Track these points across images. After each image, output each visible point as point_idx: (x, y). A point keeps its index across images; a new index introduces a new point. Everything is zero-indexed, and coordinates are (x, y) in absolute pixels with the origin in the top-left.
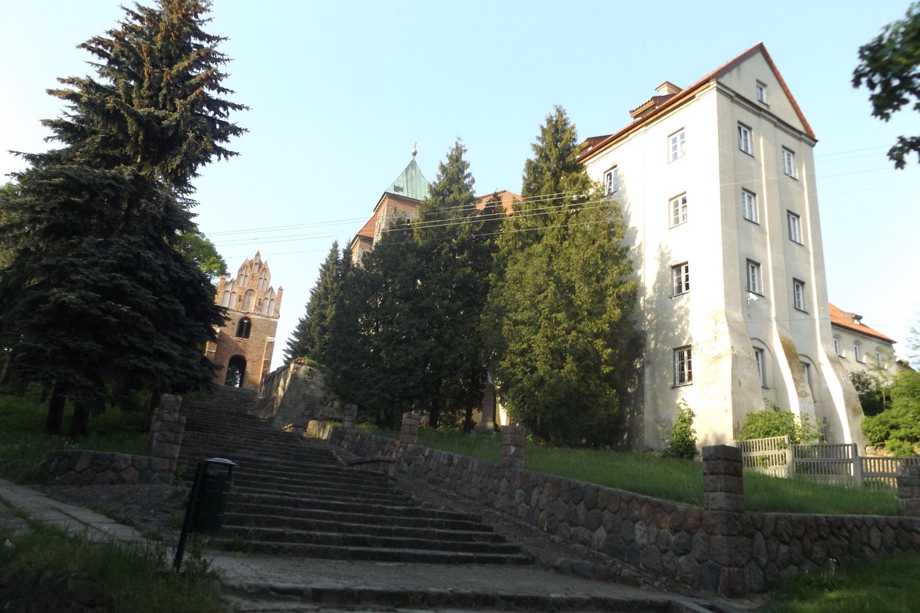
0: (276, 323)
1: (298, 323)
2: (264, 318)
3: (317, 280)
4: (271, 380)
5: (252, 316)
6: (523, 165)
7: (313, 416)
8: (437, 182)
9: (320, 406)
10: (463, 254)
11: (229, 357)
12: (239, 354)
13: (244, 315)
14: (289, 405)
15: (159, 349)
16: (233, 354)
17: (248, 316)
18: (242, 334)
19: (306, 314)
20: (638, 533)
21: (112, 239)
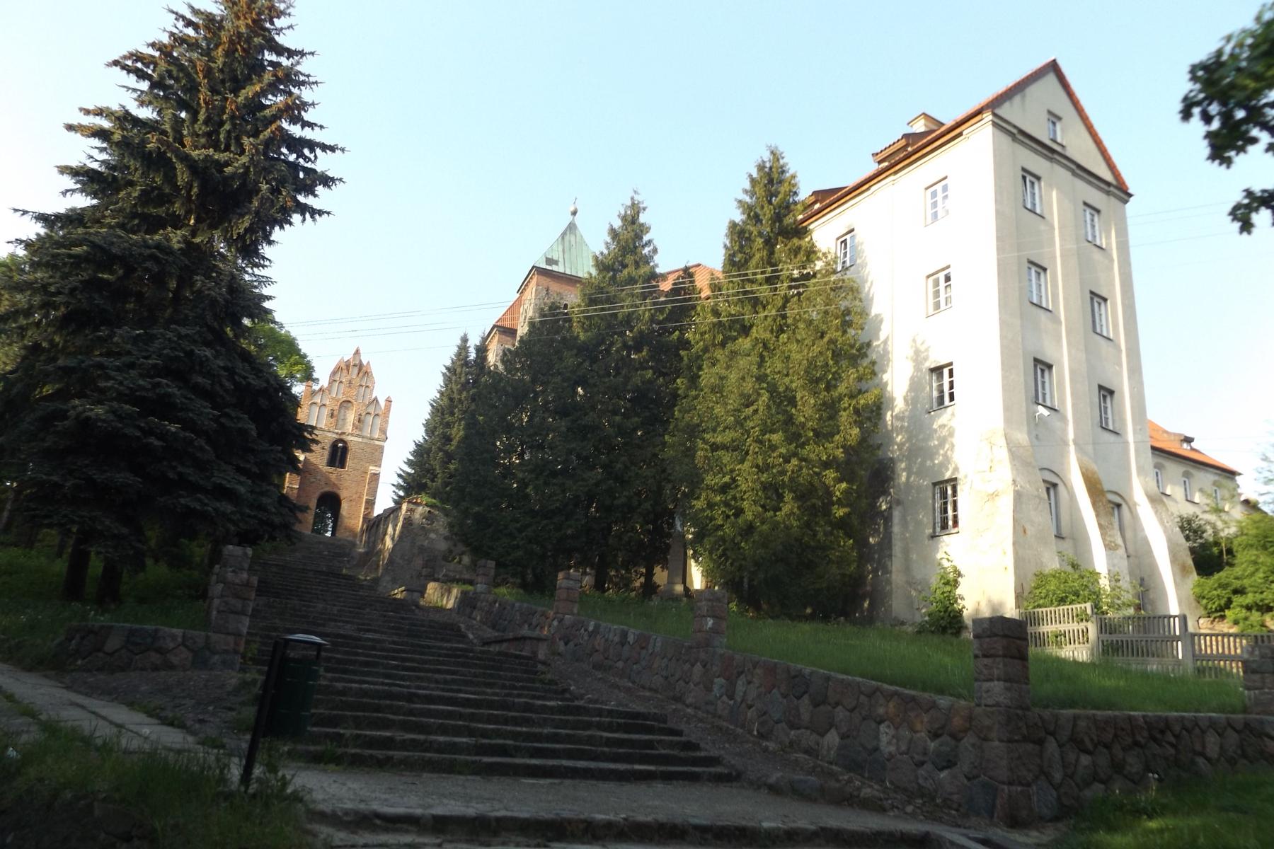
0: (382, 448)
1: (412, 447)
2: (365, 441)
3: (439, 388)
4: (375, 527)
5: (349, 438)
6: (724, 229)
7: (433, 575)
8: (606, 252)
9: (444, 563)
10: (641, 352)
11: (317, 495)
12: (331, 490)
13: (337, 437)
14: (401, 562)
15: (221, 484)
16: (322, 491)
17: (344, 437)
18: (335, 463)
19: (424, 435)
20: (884, 739)
21: (155, 331)
